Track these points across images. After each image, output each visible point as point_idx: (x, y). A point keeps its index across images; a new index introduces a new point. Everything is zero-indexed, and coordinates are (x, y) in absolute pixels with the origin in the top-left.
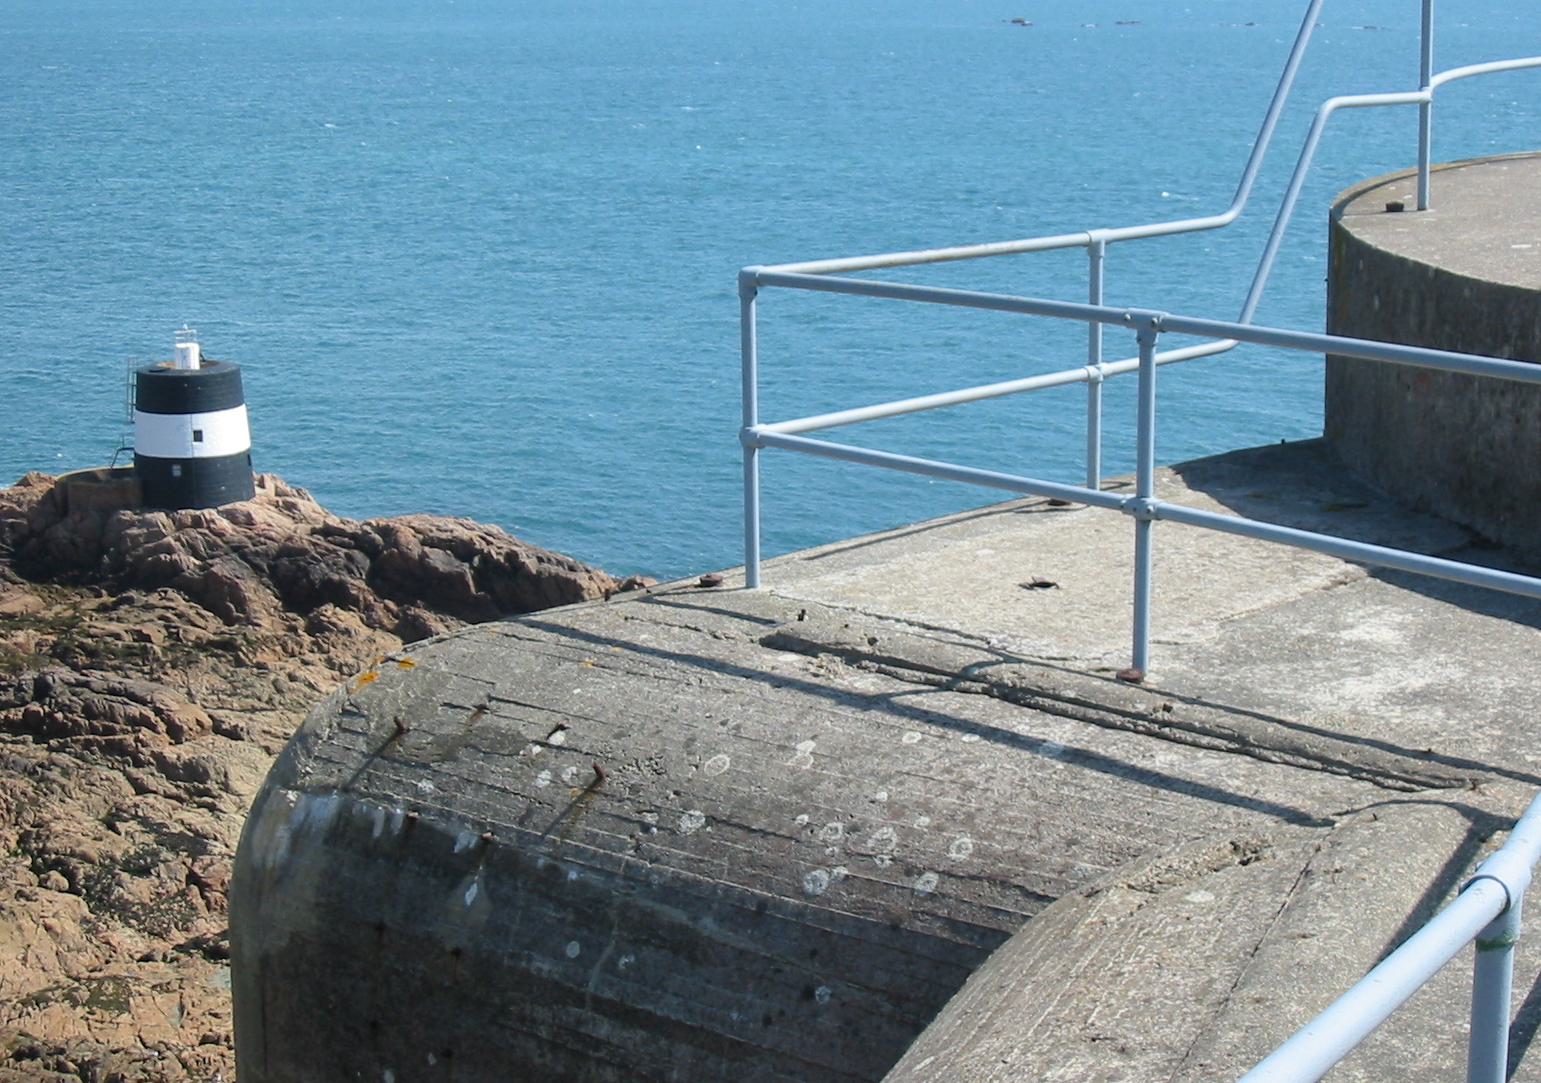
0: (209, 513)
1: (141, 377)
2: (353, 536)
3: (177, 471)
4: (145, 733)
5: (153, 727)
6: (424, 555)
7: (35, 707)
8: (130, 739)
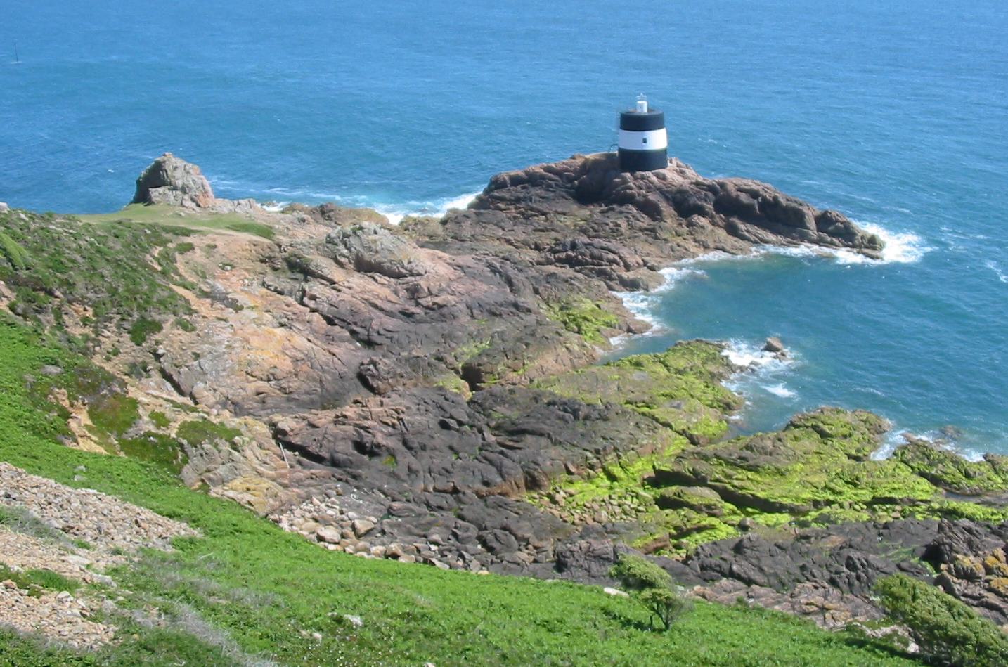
0: (648, 174)
4: (615, 266)
5: (618, 264)
6: (738, 196)
7: (570, 253)
8: (608, 269)
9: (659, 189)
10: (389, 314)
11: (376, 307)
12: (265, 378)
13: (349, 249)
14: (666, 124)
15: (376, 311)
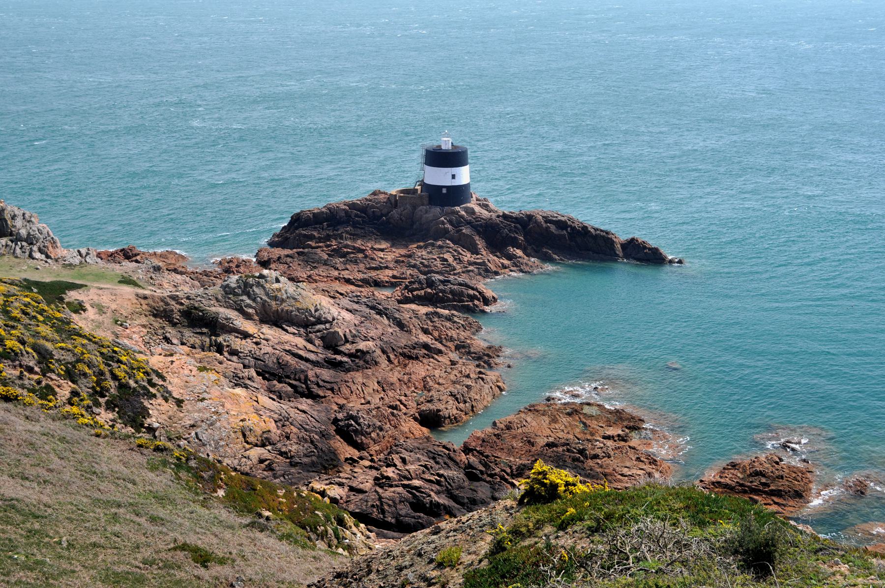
0: (457, 208)
1: (428, 151)
2: (516, 218)
3: (444, 191)
4: (476, 302)
5: (479, 300)
9: (469, 223)
10: (315, 364)
11: (300, 357)
12: (259, 443)
13: (254, 300)
14: (469, 161)
15: (303, 362)
